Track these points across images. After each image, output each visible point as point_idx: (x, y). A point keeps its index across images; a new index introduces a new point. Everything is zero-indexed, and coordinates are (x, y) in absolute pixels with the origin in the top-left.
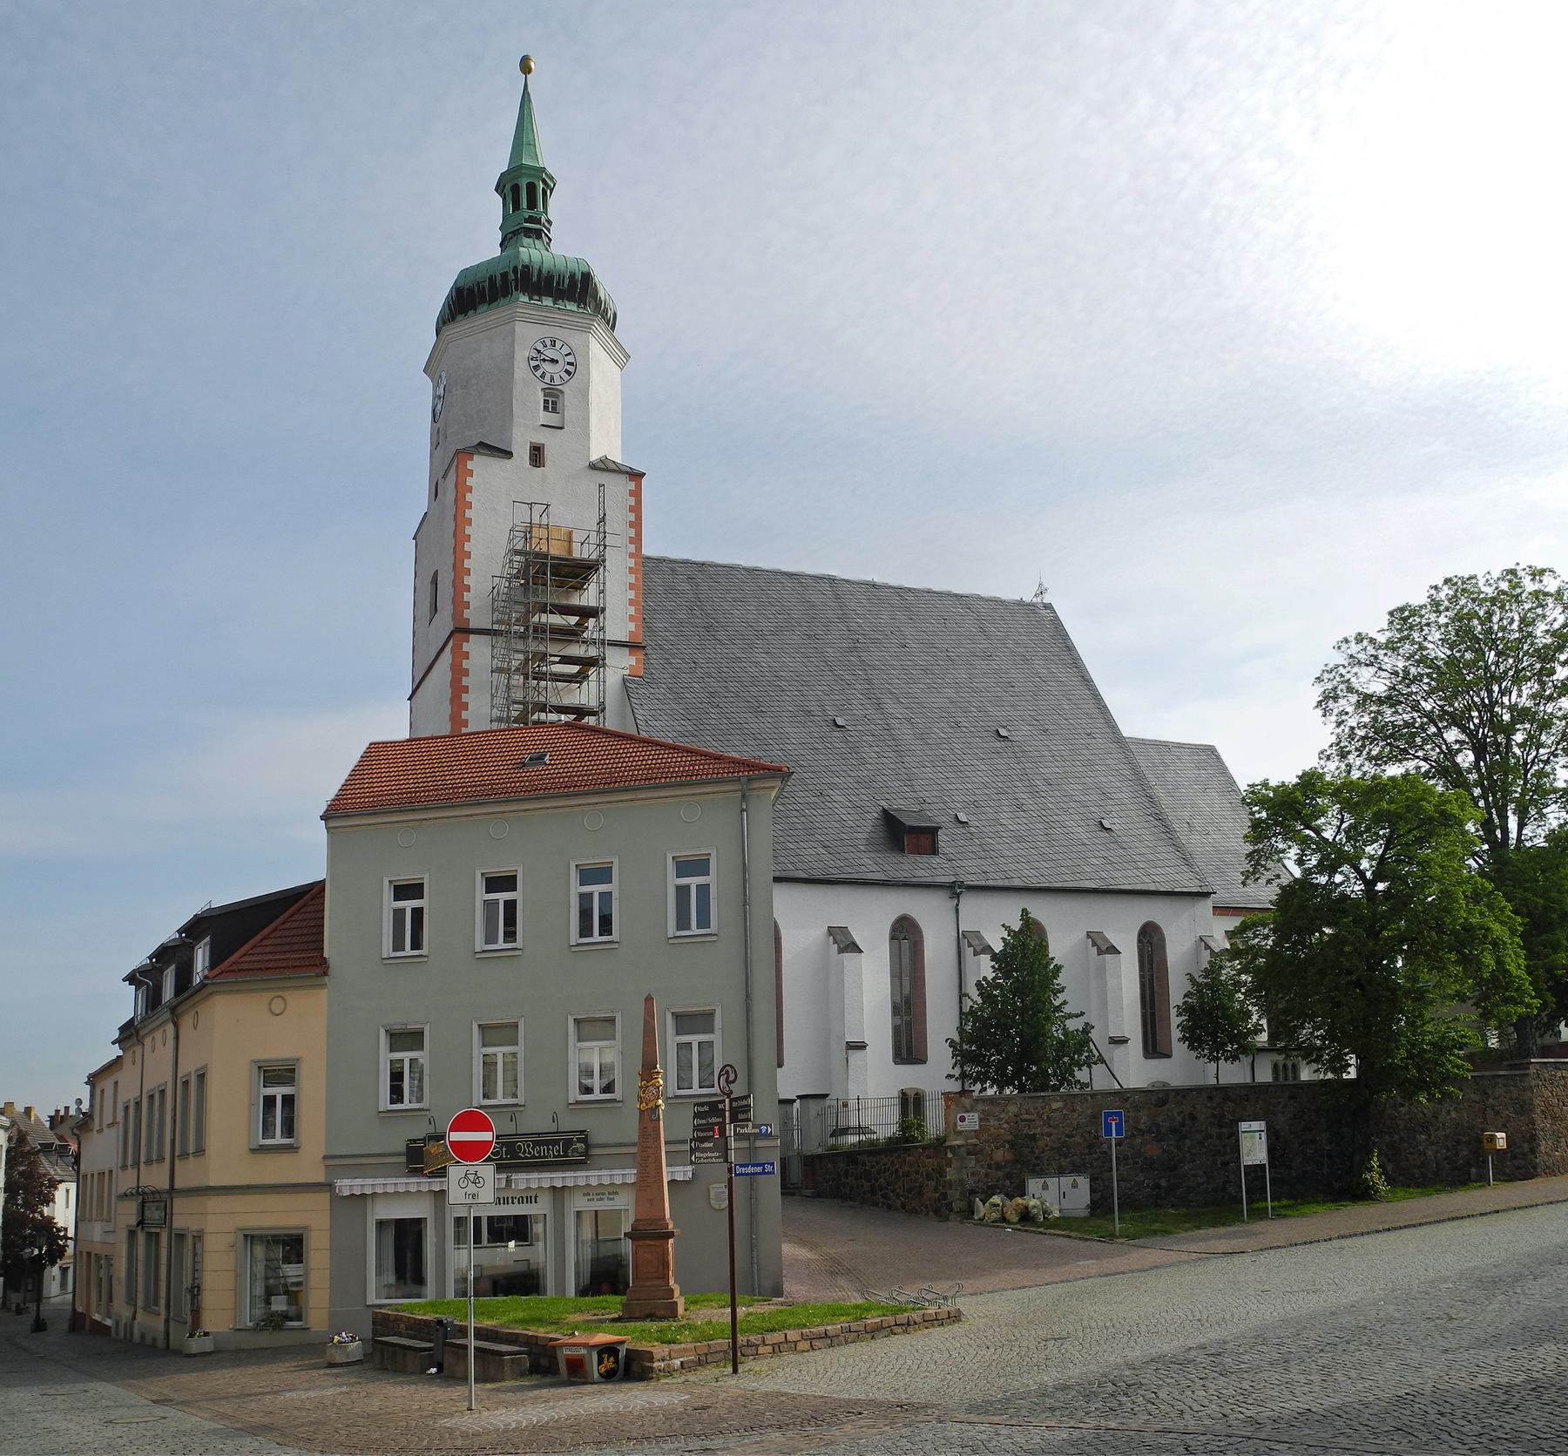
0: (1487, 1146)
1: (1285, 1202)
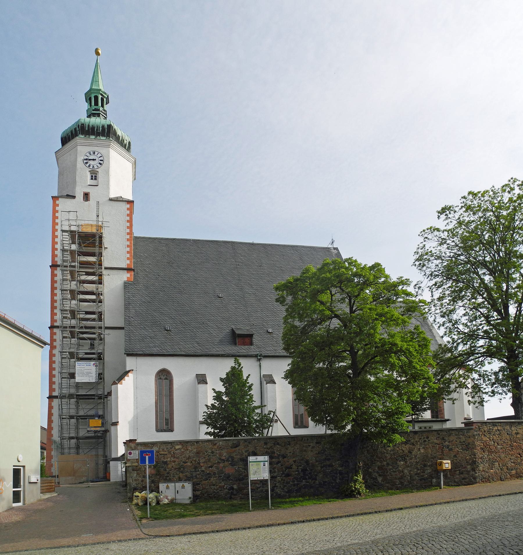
0: (439, 468)
1: (301, 499)
